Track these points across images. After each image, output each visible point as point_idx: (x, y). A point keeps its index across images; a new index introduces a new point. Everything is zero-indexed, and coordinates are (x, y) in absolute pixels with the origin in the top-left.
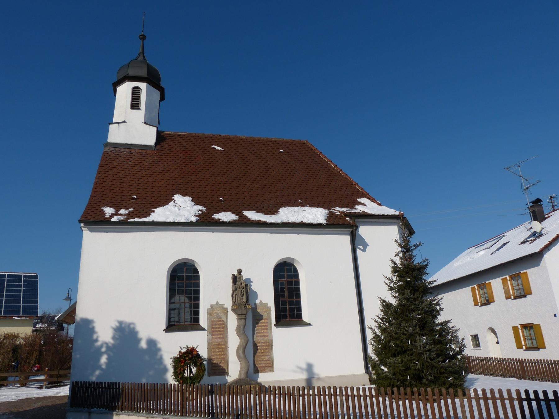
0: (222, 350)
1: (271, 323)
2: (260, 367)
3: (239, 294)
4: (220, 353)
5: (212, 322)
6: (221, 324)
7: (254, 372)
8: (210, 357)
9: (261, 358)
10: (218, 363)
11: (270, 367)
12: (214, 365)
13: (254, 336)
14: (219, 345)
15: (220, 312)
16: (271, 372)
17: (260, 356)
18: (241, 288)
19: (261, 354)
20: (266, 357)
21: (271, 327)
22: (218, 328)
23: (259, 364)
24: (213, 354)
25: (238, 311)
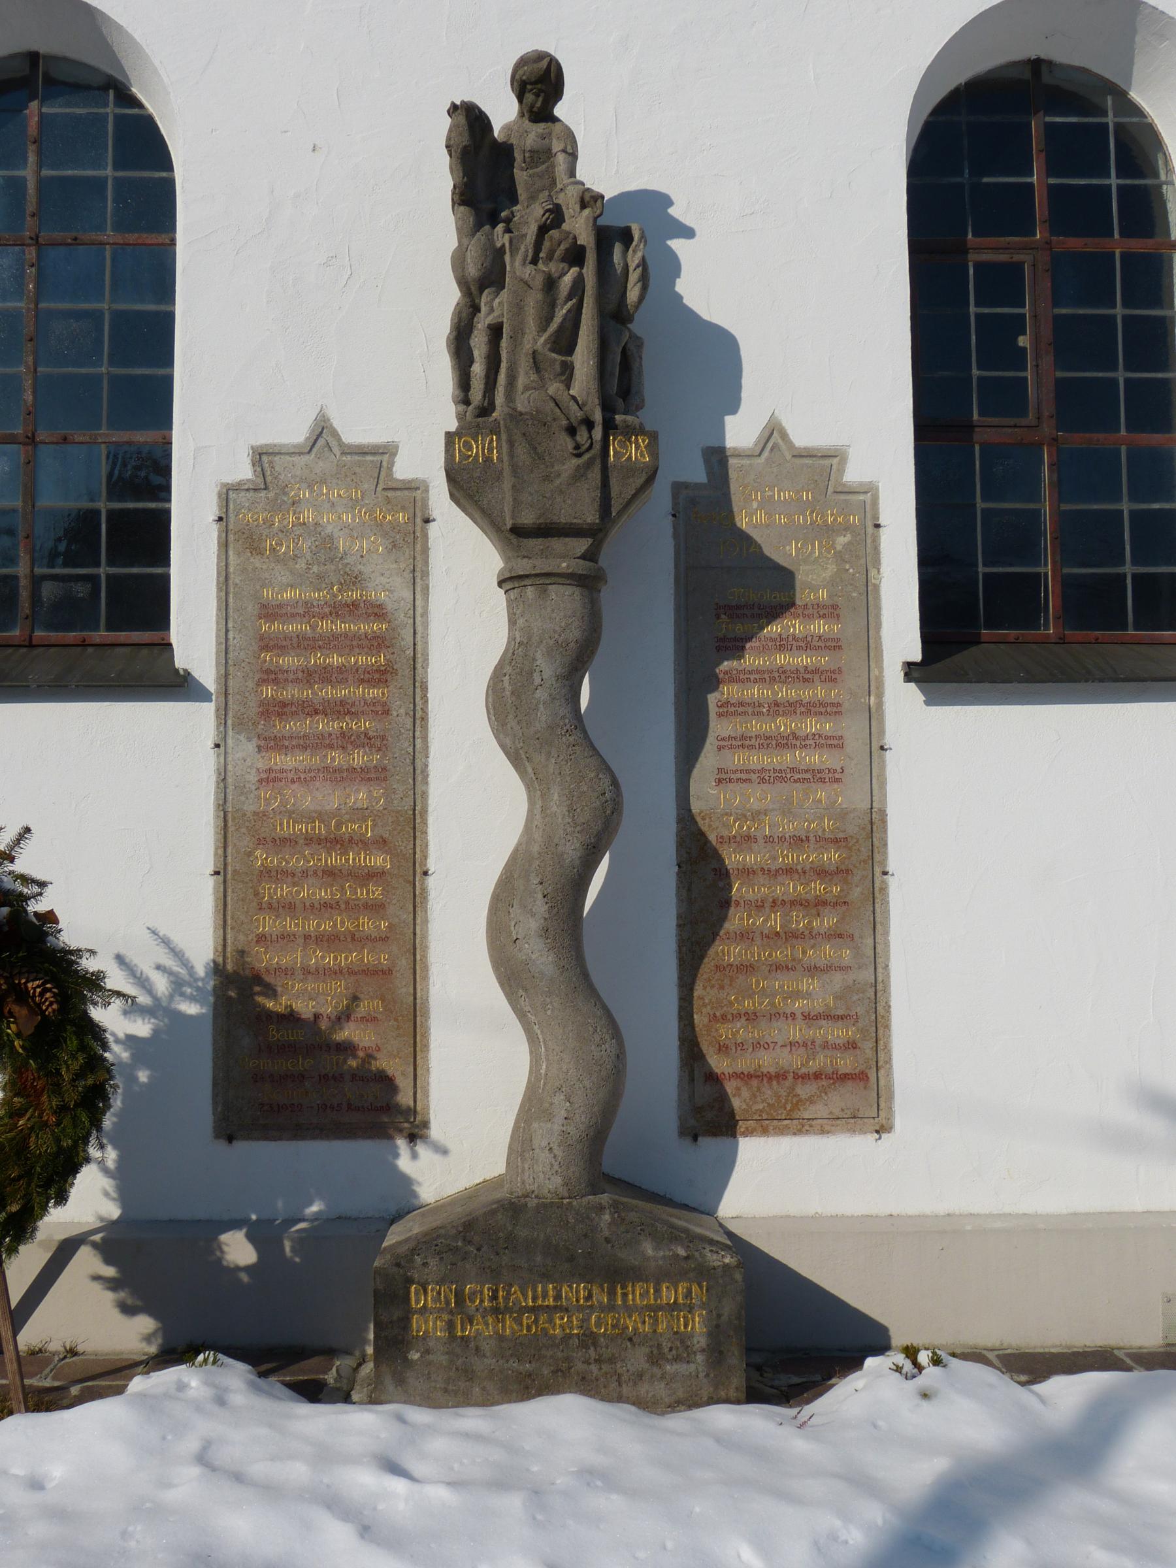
0: (362, 894)
1: (870, 648)
2: (745, 1077)
3: (531, 324)
4: (342, 923)
5: (269, 612)
6: (356, 636)
7: (682, 1120)
8: (242, 953)
9: (763, 993)
10: (317, 1016)
11: (845, 1077)
12: (275, 1034)
13: (696, 772)
14: (336, 843)
15: (348, 518)
16: (863, 1132)
17: (747, 968)
18: (550, 257)
19: (757, 953)
20: (812, 985)
21: (873, 687)
22: (326, 675)
23: (741, 1046)
24: (268, 924)
25: (503, 496)
